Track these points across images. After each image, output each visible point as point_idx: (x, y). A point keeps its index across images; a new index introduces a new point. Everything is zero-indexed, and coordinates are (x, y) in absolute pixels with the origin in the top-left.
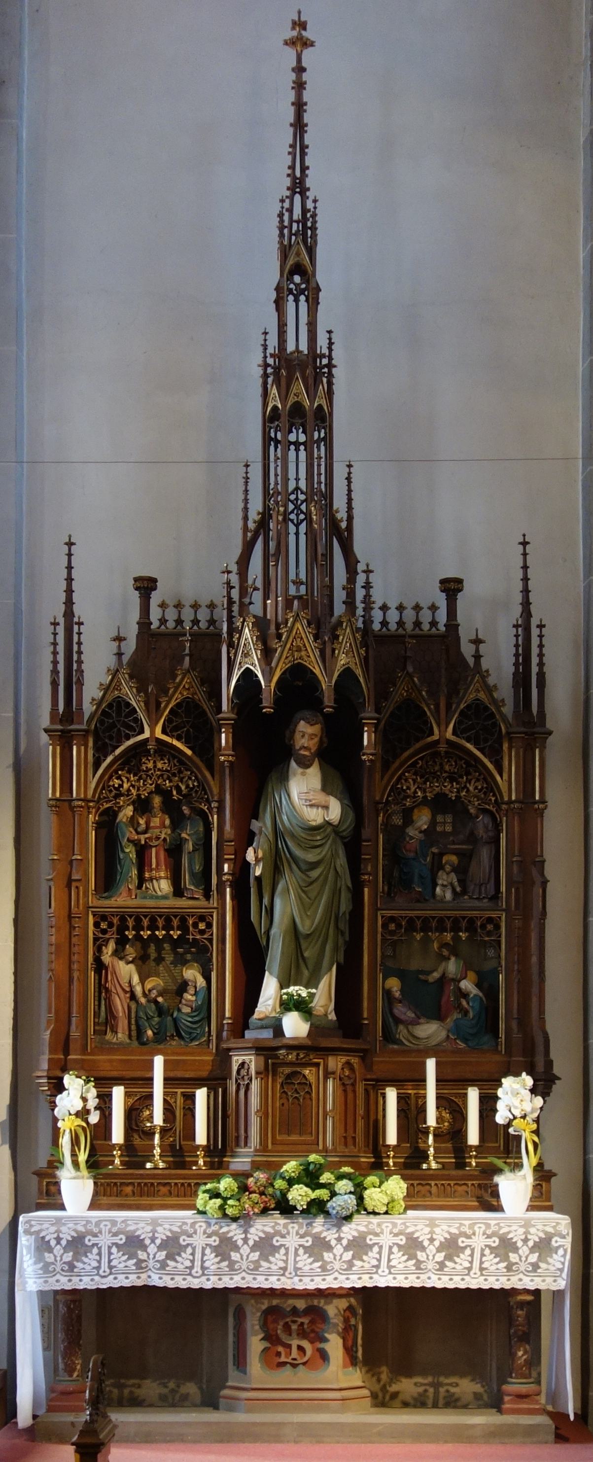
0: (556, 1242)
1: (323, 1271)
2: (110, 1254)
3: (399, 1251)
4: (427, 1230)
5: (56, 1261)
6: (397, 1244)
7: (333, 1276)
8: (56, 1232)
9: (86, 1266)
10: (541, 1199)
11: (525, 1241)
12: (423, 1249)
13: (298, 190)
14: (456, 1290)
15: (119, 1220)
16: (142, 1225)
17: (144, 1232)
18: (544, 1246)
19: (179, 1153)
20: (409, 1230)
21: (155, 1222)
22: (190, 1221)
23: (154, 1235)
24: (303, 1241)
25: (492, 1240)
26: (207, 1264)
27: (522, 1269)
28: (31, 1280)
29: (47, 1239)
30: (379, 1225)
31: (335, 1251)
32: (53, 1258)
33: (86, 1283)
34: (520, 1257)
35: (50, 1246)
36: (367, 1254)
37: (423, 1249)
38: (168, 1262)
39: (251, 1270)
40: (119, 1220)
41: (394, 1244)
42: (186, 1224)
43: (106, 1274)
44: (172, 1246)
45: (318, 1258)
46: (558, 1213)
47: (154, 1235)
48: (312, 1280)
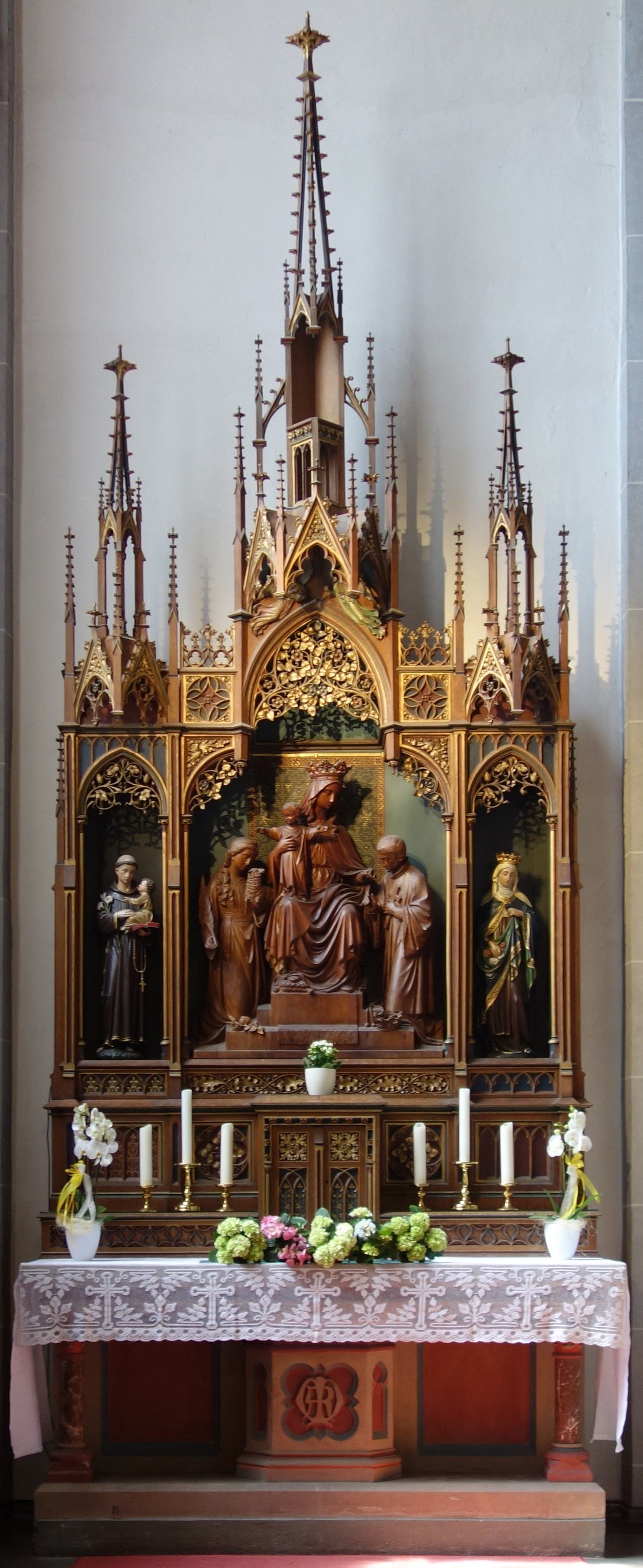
0: (440, 1291)
1: (249, 1322)
2: (428, 1306)
3: (123, 1303)
4: (154, 1279)
5: (472, 1312)
6: (330, 1296)
7: (54, 1331)
8: (157, 1282)
9: (87, 1317)
10: (588, 1245)
11: (160, 1290)
12: (257, 1299)
13: (371, 536)
14: (192, 1343)
15: (121, 1271)
16: (570, 1273)
17: (149, 1283)
18: (598, 1296)
19: (484, 1191)
20: (448, 1280)
21: (476, 1271)
22: (200, 1271)
23: (265, 1285)
24: (330, 1291)
25: (544, 1287)
26: (118, 1316)
27: (56, 1321)
28: (30, 1333)
29: (41, 1291)
30: (414, 1274)
31: (366, 1303)
32: (50, 1310)
33: (83, 1335)
34: (366, 1308)
35: (46, 1298)
36: (296, 1307)
37: (257, 1299)
38: (389, 1315)
39: (66, 1323)
40: (121, 1271)
41: (327, 1296)
42: (197, 1273)
43: (213, 1328)
44: (497, 1296)
45: (348, 1309)
46: (606, 1257)
47: (265, 1285)
48: (186, 1332)
